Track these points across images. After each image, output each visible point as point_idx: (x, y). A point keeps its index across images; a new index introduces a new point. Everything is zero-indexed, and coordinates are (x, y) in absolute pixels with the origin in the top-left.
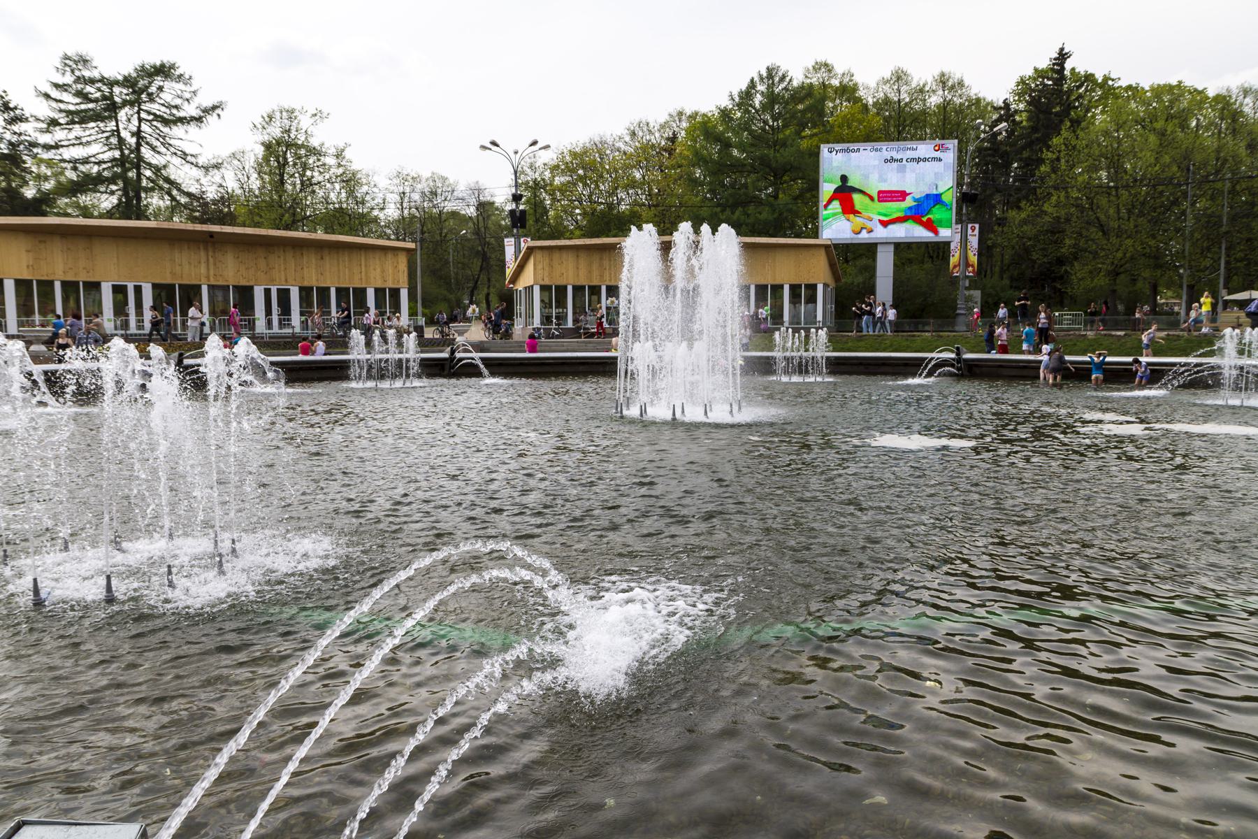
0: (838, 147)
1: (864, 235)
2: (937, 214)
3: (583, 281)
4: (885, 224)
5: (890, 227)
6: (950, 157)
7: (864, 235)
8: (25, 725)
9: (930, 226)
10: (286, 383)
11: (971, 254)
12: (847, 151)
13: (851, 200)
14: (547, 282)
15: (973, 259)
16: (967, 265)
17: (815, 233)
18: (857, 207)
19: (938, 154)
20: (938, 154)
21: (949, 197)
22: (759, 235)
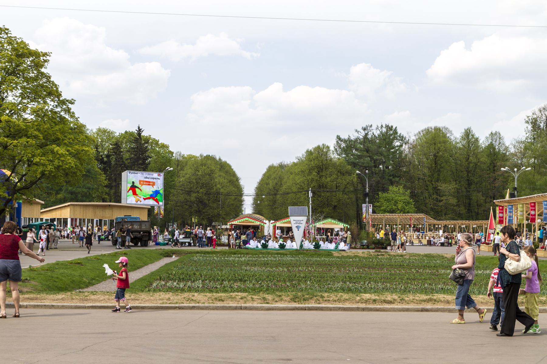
0: (132, 172)
1: (139, 203)
2: (158, 197)
3: (82, 217)
4: (145, 199)
5: (146, 200)
6: (162, 178)
7: (139, 203)
8: (220, 360)
9: (157, 201)
10: (7, 268)
11: (161, 210)
12: (134, 173)
13: (135, 190)
14: (72, 217)
15: (162, 212)
16: (160, 214)
17: (120, 201)
18: (137, 193)
19: (159, 177)
20: (159, 177)
21: (162, 192)
22: (52, 206)
